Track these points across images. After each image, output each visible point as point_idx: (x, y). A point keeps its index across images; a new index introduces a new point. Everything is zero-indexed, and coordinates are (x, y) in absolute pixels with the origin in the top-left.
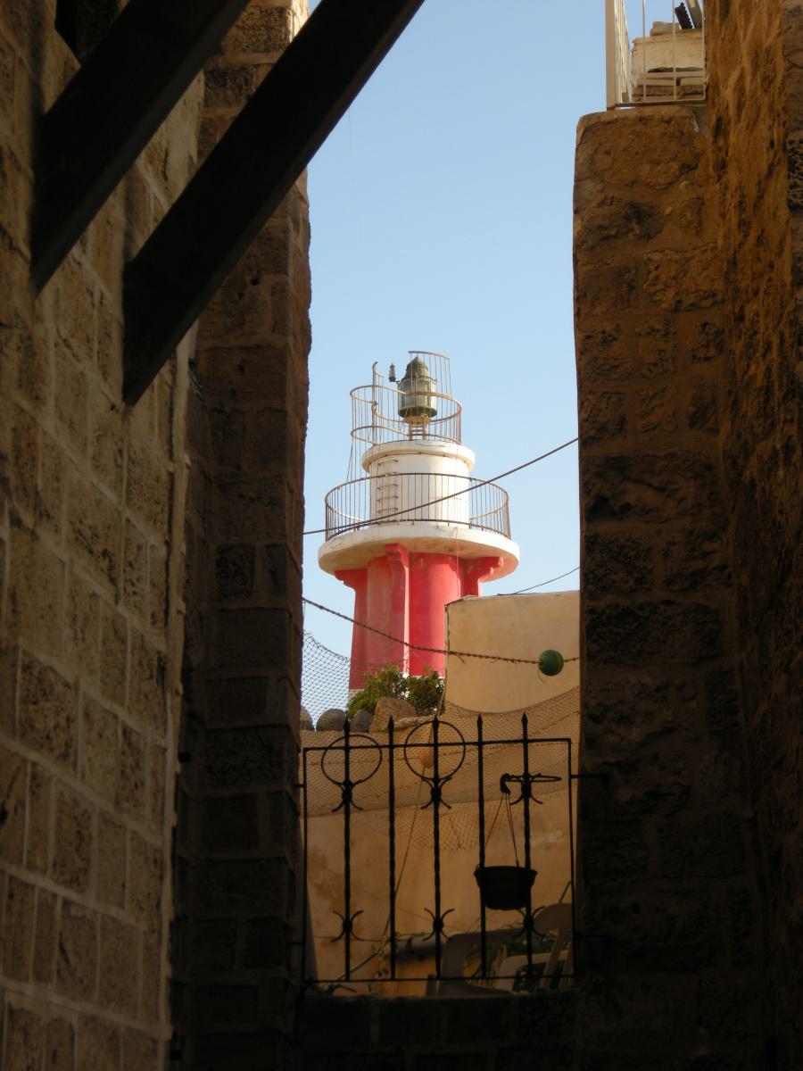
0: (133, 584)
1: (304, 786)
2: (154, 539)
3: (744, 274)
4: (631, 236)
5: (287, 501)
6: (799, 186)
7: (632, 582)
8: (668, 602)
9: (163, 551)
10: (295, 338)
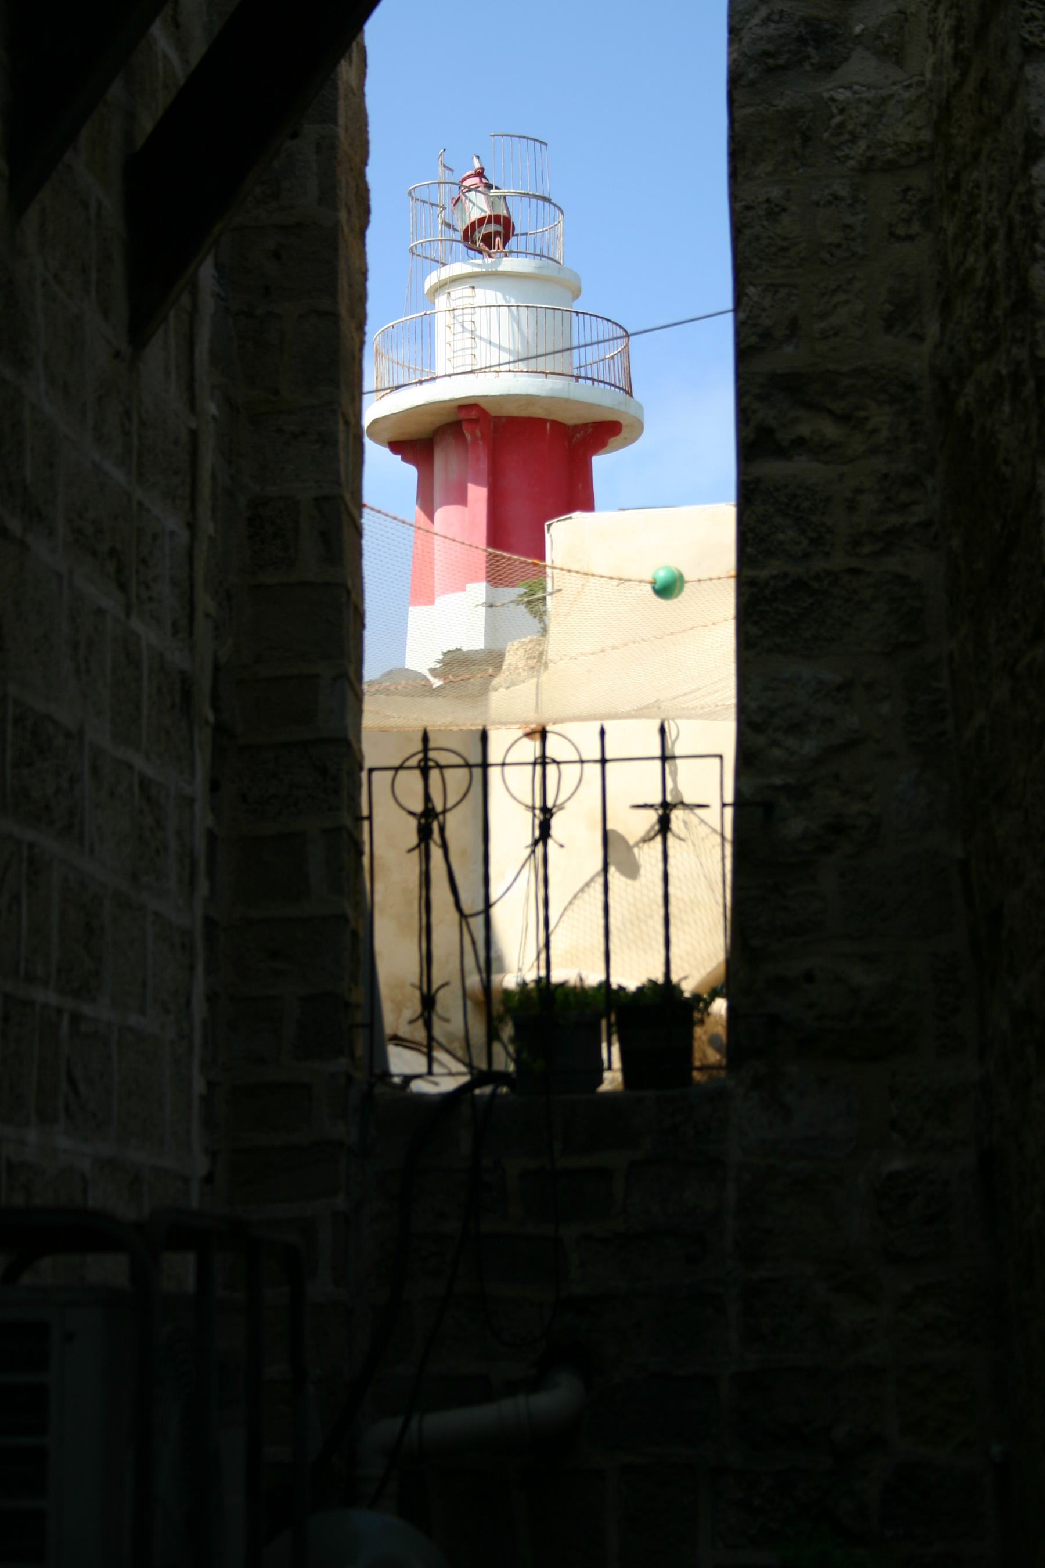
0: (148, 587)
1: (370, 818)
2: (174, 523)
3: (961, 127)
4: (807, 67)
5: (342, 437)
6: (1037, 19)
7: (805, 542)
8: (854, 571)
9: (184, 536)
10: (349, 212)
